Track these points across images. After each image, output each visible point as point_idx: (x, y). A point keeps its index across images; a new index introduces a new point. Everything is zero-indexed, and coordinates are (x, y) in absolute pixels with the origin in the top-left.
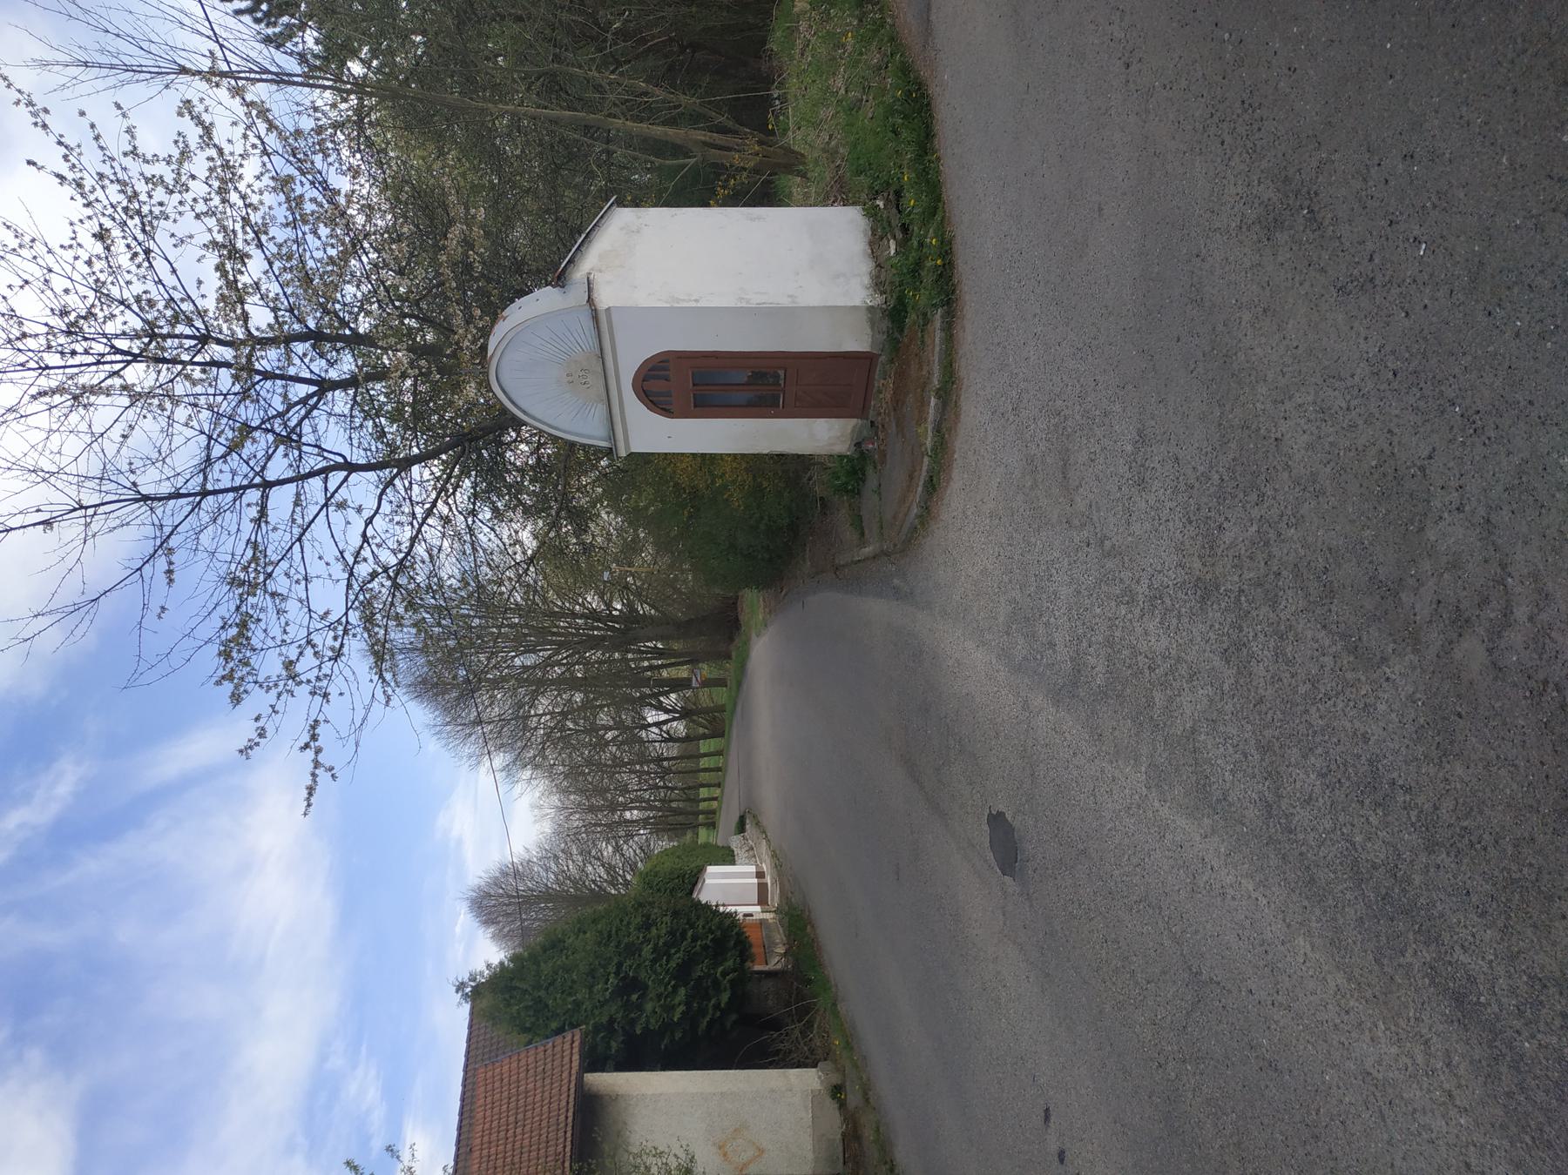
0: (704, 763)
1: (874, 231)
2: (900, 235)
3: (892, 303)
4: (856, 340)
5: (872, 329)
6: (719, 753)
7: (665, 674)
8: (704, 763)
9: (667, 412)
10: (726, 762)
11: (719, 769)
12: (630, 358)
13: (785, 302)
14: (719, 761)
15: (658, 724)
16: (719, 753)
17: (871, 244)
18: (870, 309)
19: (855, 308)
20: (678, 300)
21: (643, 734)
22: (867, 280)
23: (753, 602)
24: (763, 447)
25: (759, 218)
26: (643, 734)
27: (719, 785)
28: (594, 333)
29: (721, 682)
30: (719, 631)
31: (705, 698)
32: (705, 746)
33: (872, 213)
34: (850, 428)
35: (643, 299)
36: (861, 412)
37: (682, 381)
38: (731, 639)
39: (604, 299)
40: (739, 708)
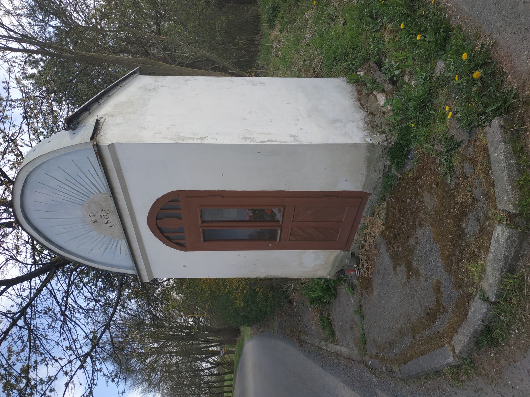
0: (226, 383)
1: (359, 92)
2: (389, 87)
3: (394, 138)
4: (347, 180)
5: (368, 167)
6: (231, 380)
7: (210, 349)
8: (226, 383)
9: (181, 246)
10: (234, 383)
11: (231, 386)
12: (141, 202)
13: (288, 140)
14: (231, 382)
15: (208, 369)
16: (231, 380)
17: (358, 100)
18: (371, 147)
19: (355, 146)
20: (183, 138)
21: (202, 373)
22: (362, 124)
23: (247, 331)
24: (261, 273)
25: (260, 84)
26: (202, 373)
27: (231, 392)
28: (101, 174)
29: (232, 353)
30: (231, 335)
31: (227, 358)
32: (226, 377)
33: (357, 82)
34: (332, 258)
35: (148, 137)
36: (345, 247)
37: (184, 217)
38: (237, 336)
39: (107, 138)
40: (239, 365)
